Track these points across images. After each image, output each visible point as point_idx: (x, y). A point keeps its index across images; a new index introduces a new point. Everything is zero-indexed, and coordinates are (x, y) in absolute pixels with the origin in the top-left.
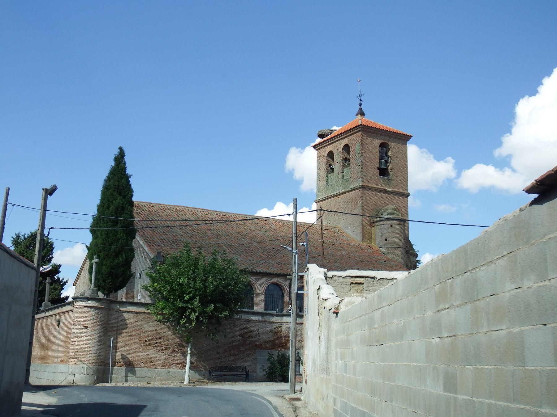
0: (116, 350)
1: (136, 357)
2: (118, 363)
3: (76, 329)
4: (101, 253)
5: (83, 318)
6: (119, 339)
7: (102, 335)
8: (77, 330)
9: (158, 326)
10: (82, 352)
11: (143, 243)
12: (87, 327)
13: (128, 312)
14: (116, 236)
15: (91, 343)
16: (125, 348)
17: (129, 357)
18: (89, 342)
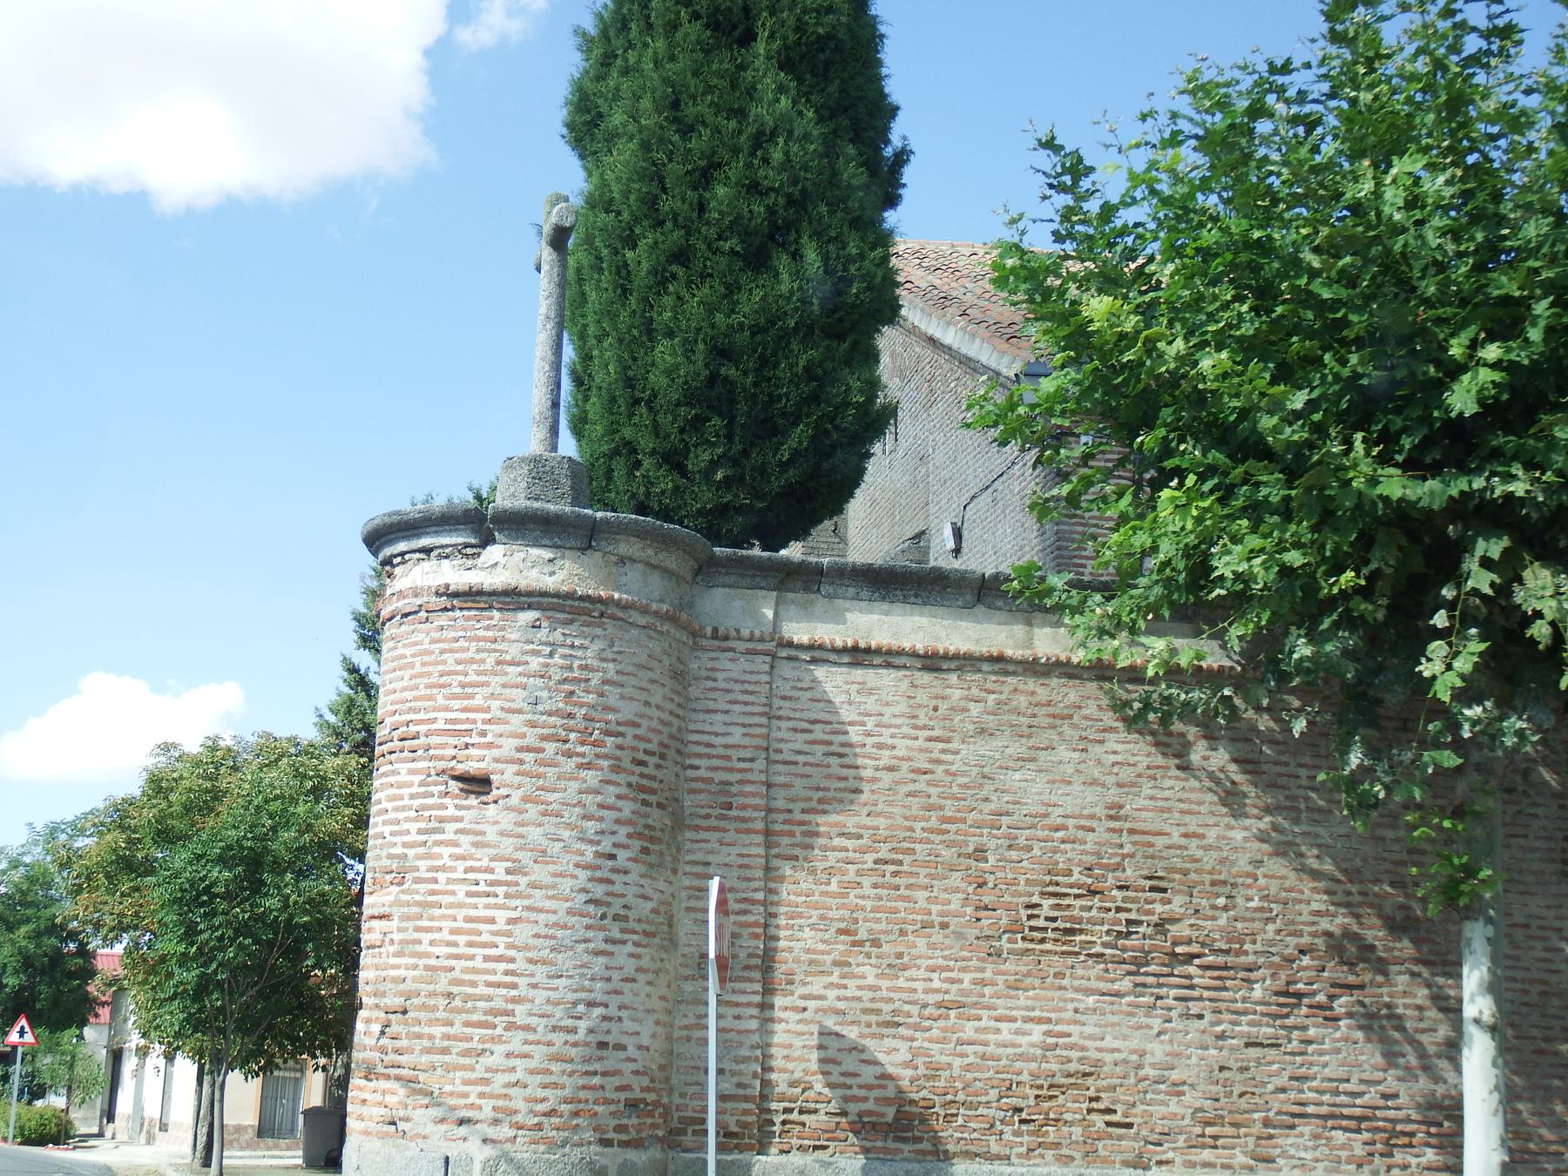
0: (768, 990)
1: (957, 1062)
2: (787, 1111)
3: (389, 806)
4: (634, 247)
5: (441, 701)
6: (785, 889)
7: (622, 855)
8: (401, 815)
9: (1126, 774)
10: (440, 1015)
11: (960, 334)
12: (477, 784)
13: (859, 655)
14: (741, 113)
15: (523, 933)
16: (853, 976)
17: (893, 1055)
18: (502, 916)
